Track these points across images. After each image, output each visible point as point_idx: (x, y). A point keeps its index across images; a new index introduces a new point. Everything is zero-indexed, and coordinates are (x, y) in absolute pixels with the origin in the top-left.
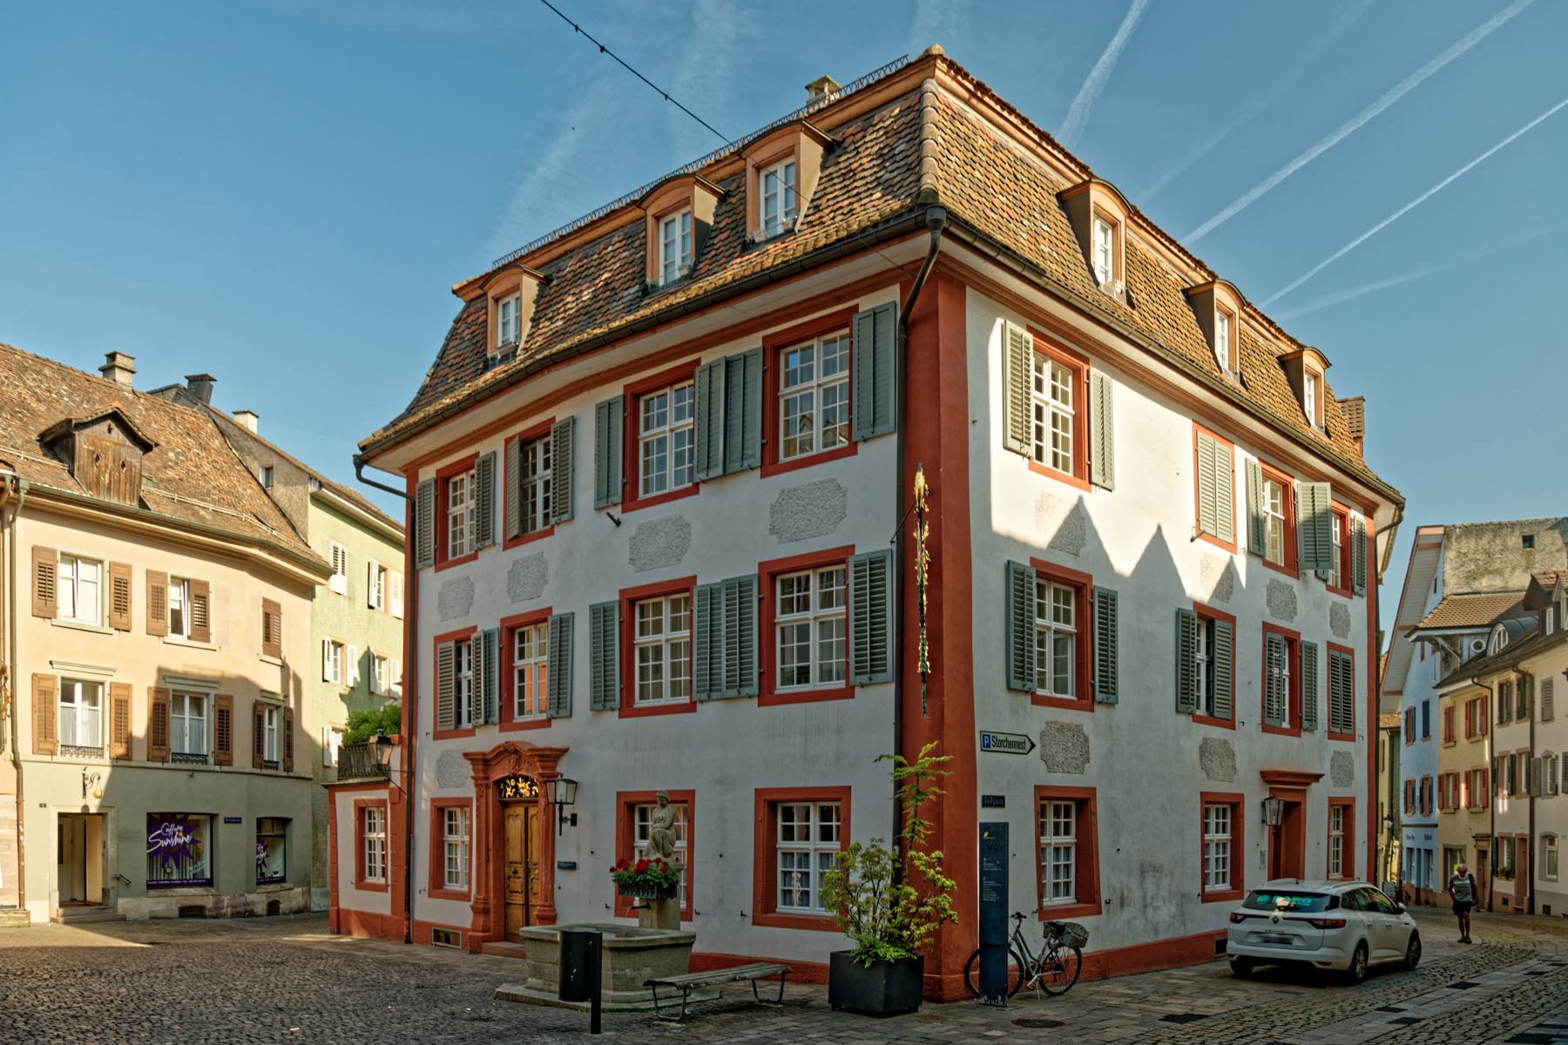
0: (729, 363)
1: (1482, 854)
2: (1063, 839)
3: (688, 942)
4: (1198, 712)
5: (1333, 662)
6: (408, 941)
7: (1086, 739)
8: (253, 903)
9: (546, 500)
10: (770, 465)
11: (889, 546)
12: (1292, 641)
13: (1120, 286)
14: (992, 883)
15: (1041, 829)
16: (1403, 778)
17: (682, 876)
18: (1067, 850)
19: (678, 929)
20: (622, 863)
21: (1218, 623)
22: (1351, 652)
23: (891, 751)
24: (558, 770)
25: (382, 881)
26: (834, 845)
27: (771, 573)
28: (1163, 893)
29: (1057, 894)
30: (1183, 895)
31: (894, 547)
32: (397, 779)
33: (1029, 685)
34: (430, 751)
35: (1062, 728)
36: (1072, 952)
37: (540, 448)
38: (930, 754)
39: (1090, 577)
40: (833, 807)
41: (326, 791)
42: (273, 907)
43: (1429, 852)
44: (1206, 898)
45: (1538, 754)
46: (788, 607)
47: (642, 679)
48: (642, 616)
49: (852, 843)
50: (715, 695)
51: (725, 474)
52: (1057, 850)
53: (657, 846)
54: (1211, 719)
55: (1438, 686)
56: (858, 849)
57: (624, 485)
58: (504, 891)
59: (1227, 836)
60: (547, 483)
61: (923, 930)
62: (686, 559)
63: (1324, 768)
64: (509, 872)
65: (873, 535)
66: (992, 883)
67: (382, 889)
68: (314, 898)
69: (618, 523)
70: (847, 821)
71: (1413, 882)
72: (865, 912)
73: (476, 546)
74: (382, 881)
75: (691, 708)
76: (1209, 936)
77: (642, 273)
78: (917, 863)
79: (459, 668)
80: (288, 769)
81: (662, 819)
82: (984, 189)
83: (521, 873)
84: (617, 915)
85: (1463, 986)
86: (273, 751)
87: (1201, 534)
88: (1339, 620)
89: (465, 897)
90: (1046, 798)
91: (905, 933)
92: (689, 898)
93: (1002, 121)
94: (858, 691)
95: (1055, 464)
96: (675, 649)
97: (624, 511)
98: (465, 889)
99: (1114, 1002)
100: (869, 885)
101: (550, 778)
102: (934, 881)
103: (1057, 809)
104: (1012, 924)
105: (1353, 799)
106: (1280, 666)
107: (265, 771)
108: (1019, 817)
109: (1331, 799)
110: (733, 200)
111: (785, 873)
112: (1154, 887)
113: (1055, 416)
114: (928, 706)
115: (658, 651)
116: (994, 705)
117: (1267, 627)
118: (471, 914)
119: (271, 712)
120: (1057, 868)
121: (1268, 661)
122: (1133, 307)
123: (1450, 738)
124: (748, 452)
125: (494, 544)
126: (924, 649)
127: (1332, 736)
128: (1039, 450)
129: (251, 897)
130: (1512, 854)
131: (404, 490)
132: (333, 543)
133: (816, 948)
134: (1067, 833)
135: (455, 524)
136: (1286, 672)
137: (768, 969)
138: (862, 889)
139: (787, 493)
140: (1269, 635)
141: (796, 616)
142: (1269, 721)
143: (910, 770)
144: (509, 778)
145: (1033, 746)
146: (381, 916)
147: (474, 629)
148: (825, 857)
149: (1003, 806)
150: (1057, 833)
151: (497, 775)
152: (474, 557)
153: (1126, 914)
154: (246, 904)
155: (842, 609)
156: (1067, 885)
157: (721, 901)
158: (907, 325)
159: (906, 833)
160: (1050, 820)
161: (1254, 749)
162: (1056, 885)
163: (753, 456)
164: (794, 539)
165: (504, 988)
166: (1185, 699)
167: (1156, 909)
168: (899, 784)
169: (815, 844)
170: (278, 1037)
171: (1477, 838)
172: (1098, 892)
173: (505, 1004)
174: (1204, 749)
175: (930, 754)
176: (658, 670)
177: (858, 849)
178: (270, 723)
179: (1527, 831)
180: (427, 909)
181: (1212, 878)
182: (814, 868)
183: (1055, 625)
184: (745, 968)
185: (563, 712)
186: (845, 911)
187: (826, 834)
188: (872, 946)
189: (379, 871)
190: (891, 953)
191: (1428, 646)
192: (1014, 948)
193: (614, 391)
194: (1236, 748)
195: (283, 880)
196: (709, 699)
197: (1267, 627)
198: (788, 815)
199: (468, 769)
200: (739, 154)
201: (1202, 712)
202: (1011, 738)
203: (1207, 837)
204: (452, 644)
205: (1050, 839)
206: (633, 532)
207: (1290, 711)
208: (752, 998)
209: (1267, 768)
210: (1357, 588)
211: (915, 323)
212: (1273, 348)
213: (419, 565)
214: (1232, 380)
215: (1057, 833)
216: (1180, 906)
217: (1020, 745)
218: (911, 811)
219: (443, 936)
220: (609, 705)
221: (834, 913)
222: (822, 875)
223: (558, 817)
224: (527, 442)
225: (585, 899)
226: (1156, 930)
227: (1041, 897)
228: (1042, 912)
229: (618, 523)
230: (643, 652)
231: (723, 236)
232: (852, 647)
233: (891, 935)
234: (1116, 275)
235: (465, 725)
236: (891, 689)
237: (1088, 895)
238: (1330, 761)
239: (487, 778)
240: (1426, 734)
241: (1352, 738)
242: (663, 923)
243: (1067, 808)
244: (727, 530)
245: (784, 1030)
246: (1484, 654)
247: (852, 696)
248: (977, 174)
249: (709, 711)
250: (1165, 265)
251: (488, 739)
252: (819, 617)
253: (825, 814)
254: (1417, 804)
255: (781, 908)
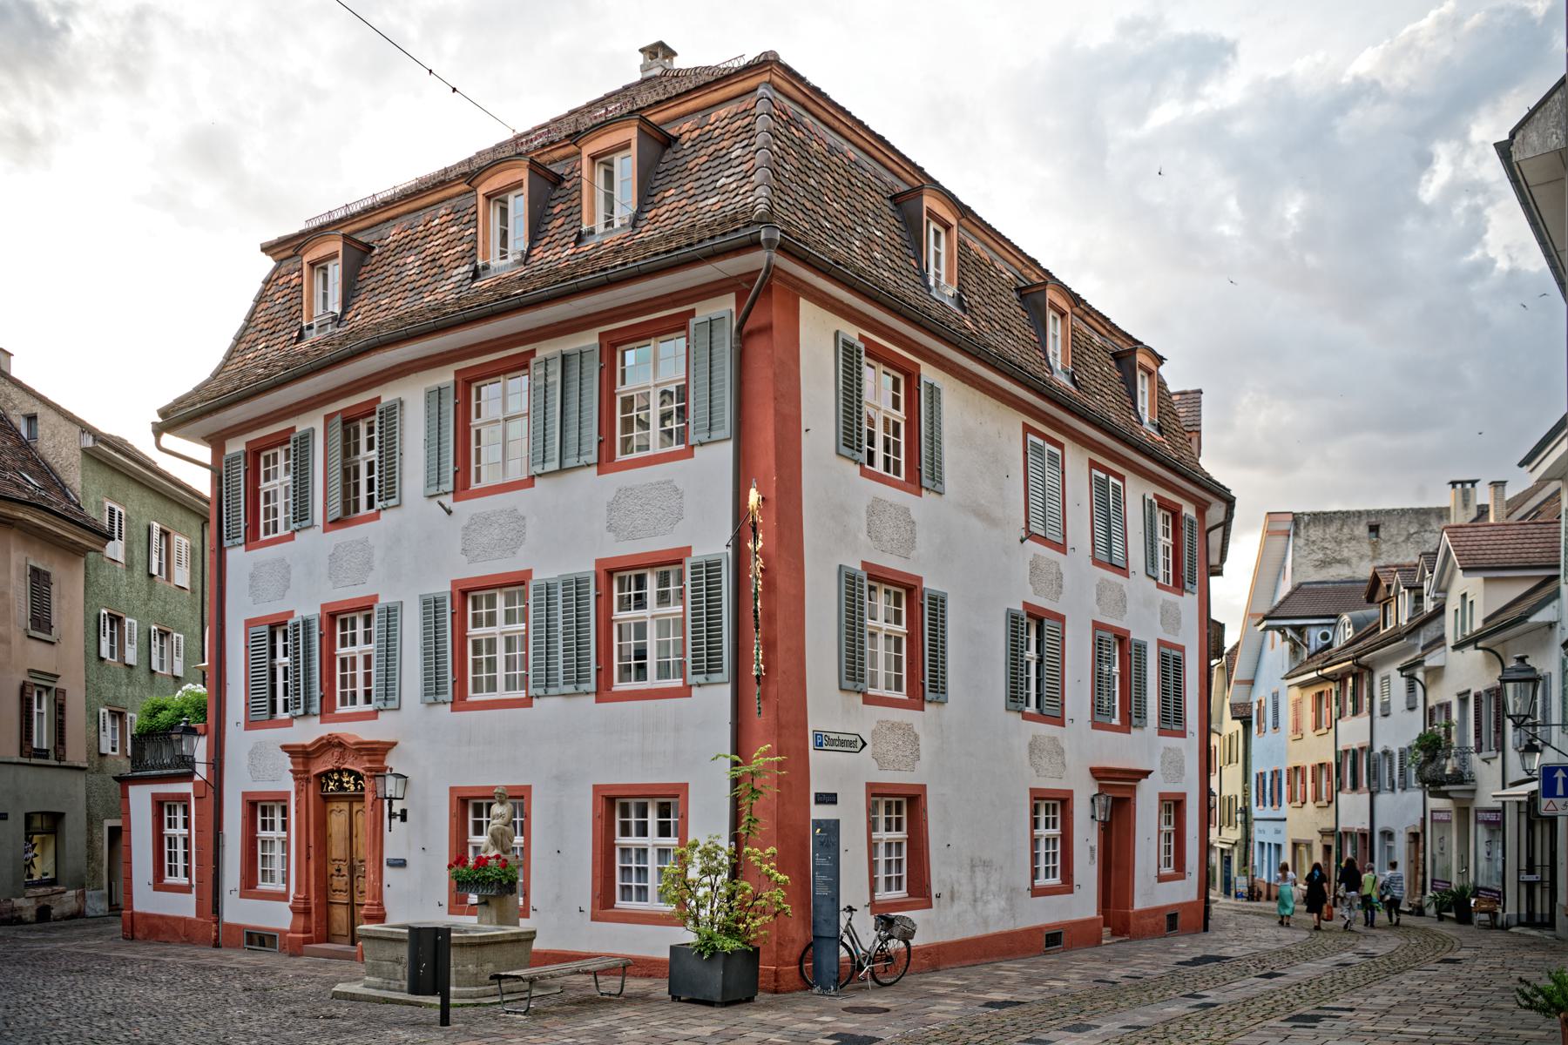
0: (565, 358)
1: (1327, 849)
2: (894, 835)
3: (531, 936)
4: (1027, 710)
5: (1163, 659)
6: (217, 945)
7: (917, 737)
8: (21, 909)
9: (371, 483)
10: (605, 461)
11: (724, 550)
12: (1122, 638)
13: (952, 290)
14: (824, 878)
15: (872, 826)
16: (1255, 770)
17: (521, 872)
18: (899, 845)
19: (517, 924)
20: (459, 860)
21: (1047, 622)
22: (1182, 649)
23: (728, 751)
24: (386, 763)
25: (185, 881)
26: (671, 841)
27: (609, 572)
28: (993, 888)
29: (889, 888)
30: (1013, 890)
31: (730, 551)
32: (202, 771)
33: (860, 685)
34: (238, 739)
35: (893, 727)
36: (902, 944)
37: (363, 427)
38: (764, 755)
39: (920, 579)
40: (668, 804)
41: (117, 785)
42: (43, 914)
43: (1278, 847)
44: (1036, 892)
45: (1378, 749)
46: (624, 605)
47: (475, 672)
48: (475, 608)
49: (690, 840)
50: (551, 691)
51: (562, 470)
52: (889, 845)
53: (495, 841)
54: (1041, 717)
55: (1287, 678)
56: (695, 845)
57: (456, 473)
58: (324, 888)
59: (1057, 831)
60: (371, 465)
61: (758, 922)
62: (521, 552)
63: (1154, 764)
64: (332, 869)
65: (712, 541)
66: (824, 878)
67: (186, 889)
68: (89, 902)
69: (449, 512)
70: (684, 817)
71: (1265, 877)
72: (703, 906)
73: (293, 526)
74: (185, 881)
75: (527, 702)
76: (1039, 929)
77: (471, 253)
78: (752, 858)
79: (273, 654)
80: (60, 758)
81: (501, 816)
82: (816, 195)
83: (345, 871)
84: (450, 913)
85: (1269, 976)
86: (42, 737)
87: (1031, 535)
88: (1170, 617)
89: (283, 897)
90: (875, 792)
91: (741, 926)
92: (526, 895)
93: (837, 124)
94: (695, 690)
95: (887, 469)
96: (509, 642)
97: (455, 500)
98: (282, 888)
99: (941, 991)
100: (707, 880)
101: (380, 773)
102: (769, 876)
103: (888, 805)
104: (844, 918)
105: (1184, 795)
106: (1111, 663)
107: (34, 761)
108: (851, 816)
109: (1161, 795)
110: (568, 185)
111: (623, 869)
112: (984, 883)
113: (886, 420)
114: (766, 707)
115: (492, 643)
116: (826, 705)
117: (1097, 626)
118: (291, 914)
119: (40, 694)
120: (888, 863)
121: (1099, 658)
122: (964, 309)
123: (1297, 728)
124: (585, 448)
125: (312, 526)
126: (758, 653)
127: (1162, 732)
128: (871, 455)
129: (19, 902)
130: (1354, 848)
131: (208, 461)
132: (108, 504)
133: (656, 943)
134: (899, 828)
135: (267, 501)
136: (1116, 669)
137: (611, 963)
138: (700, 884)
139: (624, 492)
140: (1099, 633)
141: (634, 613)
142: (1098, 718)
143: (746, 769)
144: (332, 771)
145: (864, 744)
146: (184, 919)
147: (291, 614)
148: (663, 853)
149: (835, 802)
150: (888, 829)
151: (318, 767)
152: (291, 537)
153: (956, 908)
154: (13, 910)
155: (679, 609)
156: (899, 879)
157: (558, 898)
158: (744, 336)
159: (742, 830)
160: (882, 816)
161: (1080, 750)
162: (888, 880)
163: (590, 452)
164: (632, 537)
165: (340, 987)
166: (1015, 696)
167: (986, 903)
168: (736, 782)
169: (653, 840)
170: (121, 1038)
171: (1323, 833)
172: (929, 886)
173: (344, 1003)
174: (1034, 747)
175: (764, 755)
176: (492, 664)
177: (695, 845)
178: (39, 706)
179: (1367, 827)
180: (238, 911)
181: (1042, 872)
182: (652, 863)
183: (885, 626)
184: (587, 962)
185: (390, 704)
186: (682, 903)
187: (664, 831)
188: (710, 938)
189: (181, 871)
190: (730, 945)
191: (1278, 636)
192: (846, 940)
193: (445, 377)
194: (1065, 745)
195: (53, 882)
196: (546, 695)
197: (1097, 626)
198: (625, 812)
199: (286, 761)
200: (575, 137)
201: (1032, 709)
202: (842, 737)
203: (1036, 832)
204: (266, 628)
205: (882, 835)
206: (465, 522)
207: (1119, 707)
208: (594, 992)
209: (1096, 765)
210: (1188, 586)
211: (751, 333)
212: (1109, 345)
213: (226, 543)
214: (1063, 380)
215: (888, 829)
216: (1010, 899)
217: (853, 744)
218: (746, 808)
219: (259, 939)
220: (440, 698)
221: (671, 908)
222: (661, 871)
223: (385, 812)
224: (349, 422)
225: (416, 895)
226: (986, 922)
227: (873, 890)
228: (873, 905)
229: (449, 512)
230: (477, 644)
231: (559, 222)
232: (688, 594)
233: (728, 928)
234: (949, 280)
235: (281, 714)
236: (727, 690)
237: (920, 891)
238: (1161, 760)
239: (307, 772)
240: (1276, 726)
241: (1182, 734)
242: (503, 920)
243: (899, 805)
244: (565, 527)
245: (627, 1019)
246: (1329, 646)
247: (690, 695)
248: (812, 182)
249: (546, 707)
250: (999, 264)
251: (308, 731)
252: (659, 621)
253: (664, 811)
254: (1268, 798)
255: (619, 903)
